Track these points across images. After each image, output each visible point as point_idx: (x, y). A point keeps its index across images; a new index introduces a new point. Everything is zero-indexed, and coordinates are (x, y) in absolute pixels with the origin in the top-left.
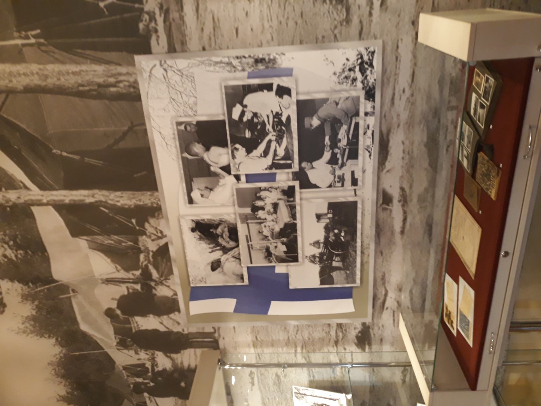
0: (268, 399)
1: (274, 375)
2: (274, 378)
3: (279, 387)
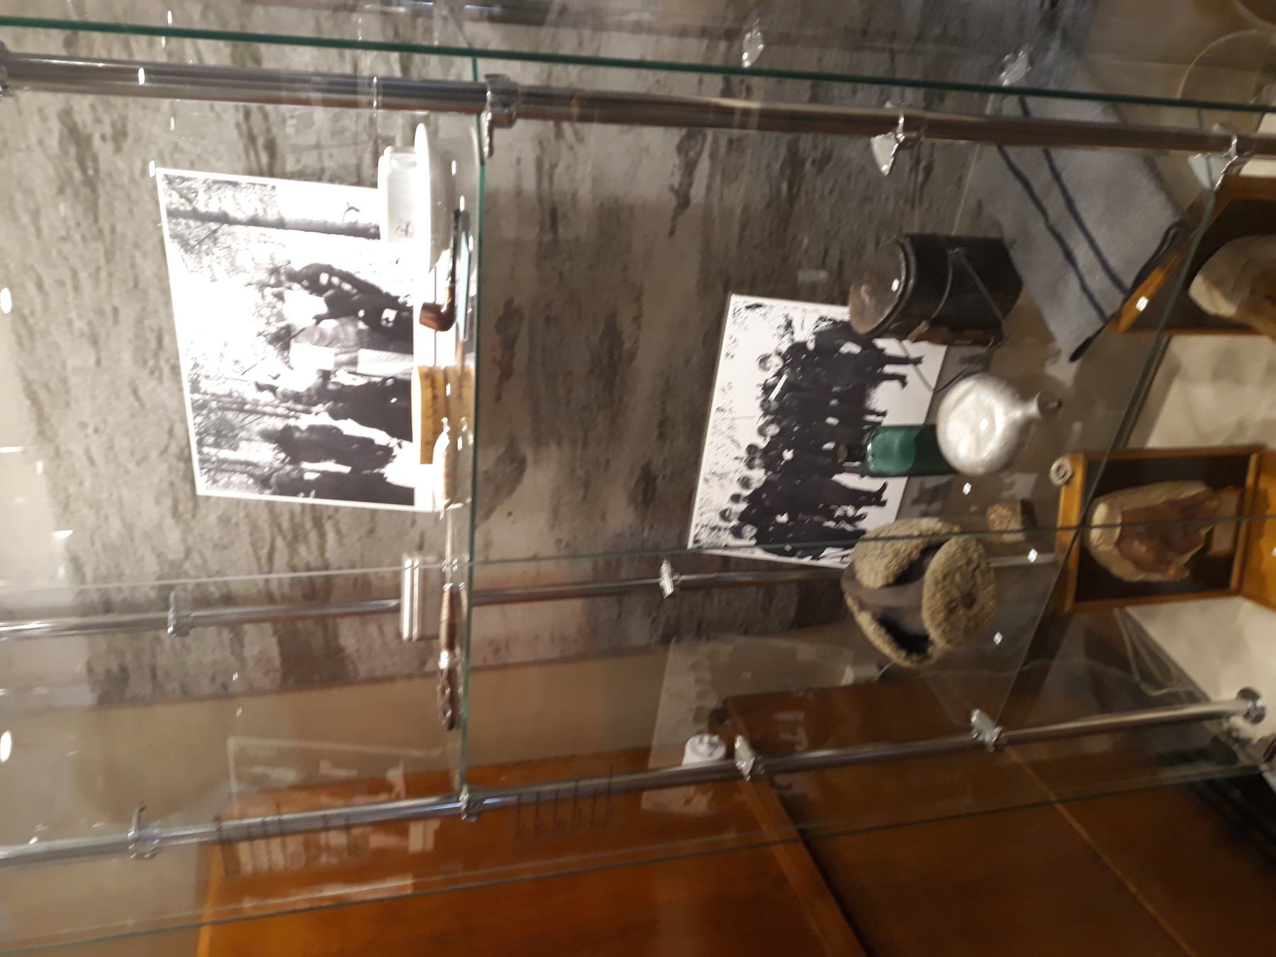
0: (40, 286)
1: (55, 125)
2: (53, 142)
3: (93, 209)
